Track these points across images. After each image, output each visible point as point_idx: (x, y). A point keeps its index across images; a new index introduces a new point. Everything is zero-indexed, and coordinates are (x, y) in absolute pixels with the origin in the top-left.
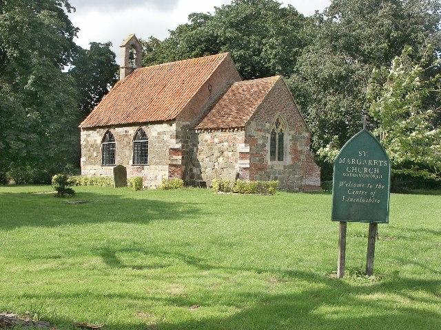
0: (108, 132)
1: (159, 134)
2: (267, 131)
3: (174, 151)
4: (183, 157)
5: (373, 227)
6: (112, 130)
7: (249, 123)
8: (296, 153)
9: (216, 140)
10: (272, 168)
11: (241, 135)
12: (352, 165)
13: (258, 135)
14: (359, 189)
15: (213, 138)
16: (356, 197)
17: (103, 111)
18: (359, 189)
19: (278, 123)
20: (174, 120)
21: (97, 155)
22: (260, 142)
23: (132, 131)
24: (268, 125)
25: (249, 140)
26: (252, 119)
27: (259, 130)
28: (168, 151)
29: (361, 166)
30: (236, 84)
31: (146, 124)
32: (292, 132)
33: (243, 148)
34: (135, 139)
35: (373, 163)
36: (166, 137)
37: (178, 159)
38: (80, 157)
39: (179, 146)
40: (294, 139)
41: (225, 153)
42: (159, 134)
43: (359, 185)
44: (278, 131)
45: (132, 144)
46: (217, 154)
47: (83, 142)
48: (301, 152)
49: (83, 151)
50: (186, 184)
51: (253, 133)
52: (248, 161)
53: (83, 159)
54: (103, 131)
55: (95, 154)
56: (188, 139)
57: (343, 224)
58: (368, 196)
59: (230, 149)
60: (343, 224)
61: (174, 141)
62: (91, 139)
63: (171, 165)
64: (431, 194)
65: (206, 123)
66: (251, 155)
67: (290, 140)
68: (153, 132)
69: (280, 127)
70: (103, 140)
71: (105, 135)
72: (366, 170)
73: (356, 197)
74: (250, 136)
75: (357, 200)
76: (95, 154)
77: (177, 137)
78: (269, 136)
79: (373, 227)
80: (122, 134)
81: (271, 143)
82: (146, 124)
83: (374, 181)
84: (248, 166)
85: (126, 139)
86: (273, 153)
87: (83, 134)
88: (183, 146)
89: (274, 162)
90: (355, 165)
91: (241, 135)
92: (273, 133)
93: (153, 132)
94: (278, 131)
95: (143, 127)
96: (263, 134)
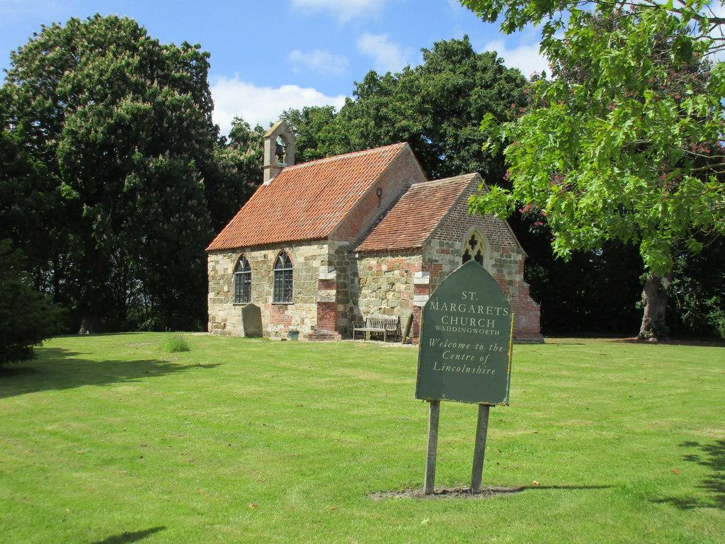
0: (241, 258)
1: (306, 259)
2: (456, 252)
3: (326, 284)
4: (338, 292)
5: (485, 409)
6: (287, 250)
7: (428, 242)
9: (384, 268)
11: (416, 260)
12: (449, 313)
13: (444, 259)
14: (462, 352)
16: (460, 363)
17: (240, 228)
18: (462, 352)
19: (473, 242)
20: (326, 238)
21: (228, 288)
23: (272, 255)
24: (458, 245)
25: (427, 267)
26: (433, 235)
27: (443, 252)
28: (317, 284)
29: (466, 315)
30: (415, 186)
31: (291, 243)
33: (421, 278)
35: (485, 310)
36: (316, 264)
38: (207, 292)
39: (332, 276)
42: (306, 259)
43: (462, 346)
44: (473, 253)
45: (272, 274)
46: (385, 287)
47: (210, 273)
49: (211, 284)
50: (248, 335)
51: (435, 255)
53: (211, 295)
54: (236, 256)
56: (344, 262)
57: (435, 405)
58: (475, 364)
60: (435, 405)
61: (325, 268)
62: (220, 266)
65: (368, 244)
68: (299, 256)
69: (477, 247)
70: (237, 268)
72: (473, 321)
73: (460, 363)
74: (431, 261)
75: (458, 369)
77: (330, 263)
79: (485, 409)
80: (259, 259)
82: (291, 243)
83: (487, 340)
85: (265, 266)
87: (211, 258)
88: (338, 276)
90: (457, 314)
93: (299, 256)
94: (473, 253)
95: (287, 250)
96: (448, 257)
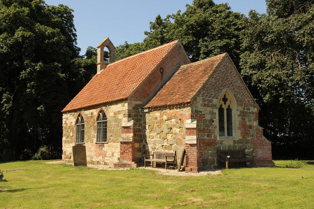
1: (115, 114)
2: (214, 106)
8: (245, 128)
9: (165, 117)
10: (222, 143)
11: (187, 111)
15: (161, 116)
20: (126, 99)
22: (208, 117)
23: (95, 112)
27: (205, 105)
31: (105, 104)
32: (241, 108)
34: (98, 119)
37: (130, 136)
40: (243, 115)
41: (174, 129)
42: (115, 114)
45: (96, 124)
46: (166, 130)
48: (250, 127)
51: (200, 108)
52: (195, 137)
55: (71, 134)
59: (178, 125)
63: (122, 143)
64: (3, 163)
65: (154, 102)
66: (199, 130)
67: (239, 115)
68: (111, 111)
70: (77, 122)
71: (78, 118)
74: (197, 111)
76: (71, 134)
78: (216, 111)
80: (89, 115)
81: (219, 118)
82: (105, 104)
84: (195, 142)
86: (221, 129)
87: (64, 116)
89: (223, 138)
91: (187, 111)
92: (221, 110)
94: (225, 107)
95: (104, 108)
